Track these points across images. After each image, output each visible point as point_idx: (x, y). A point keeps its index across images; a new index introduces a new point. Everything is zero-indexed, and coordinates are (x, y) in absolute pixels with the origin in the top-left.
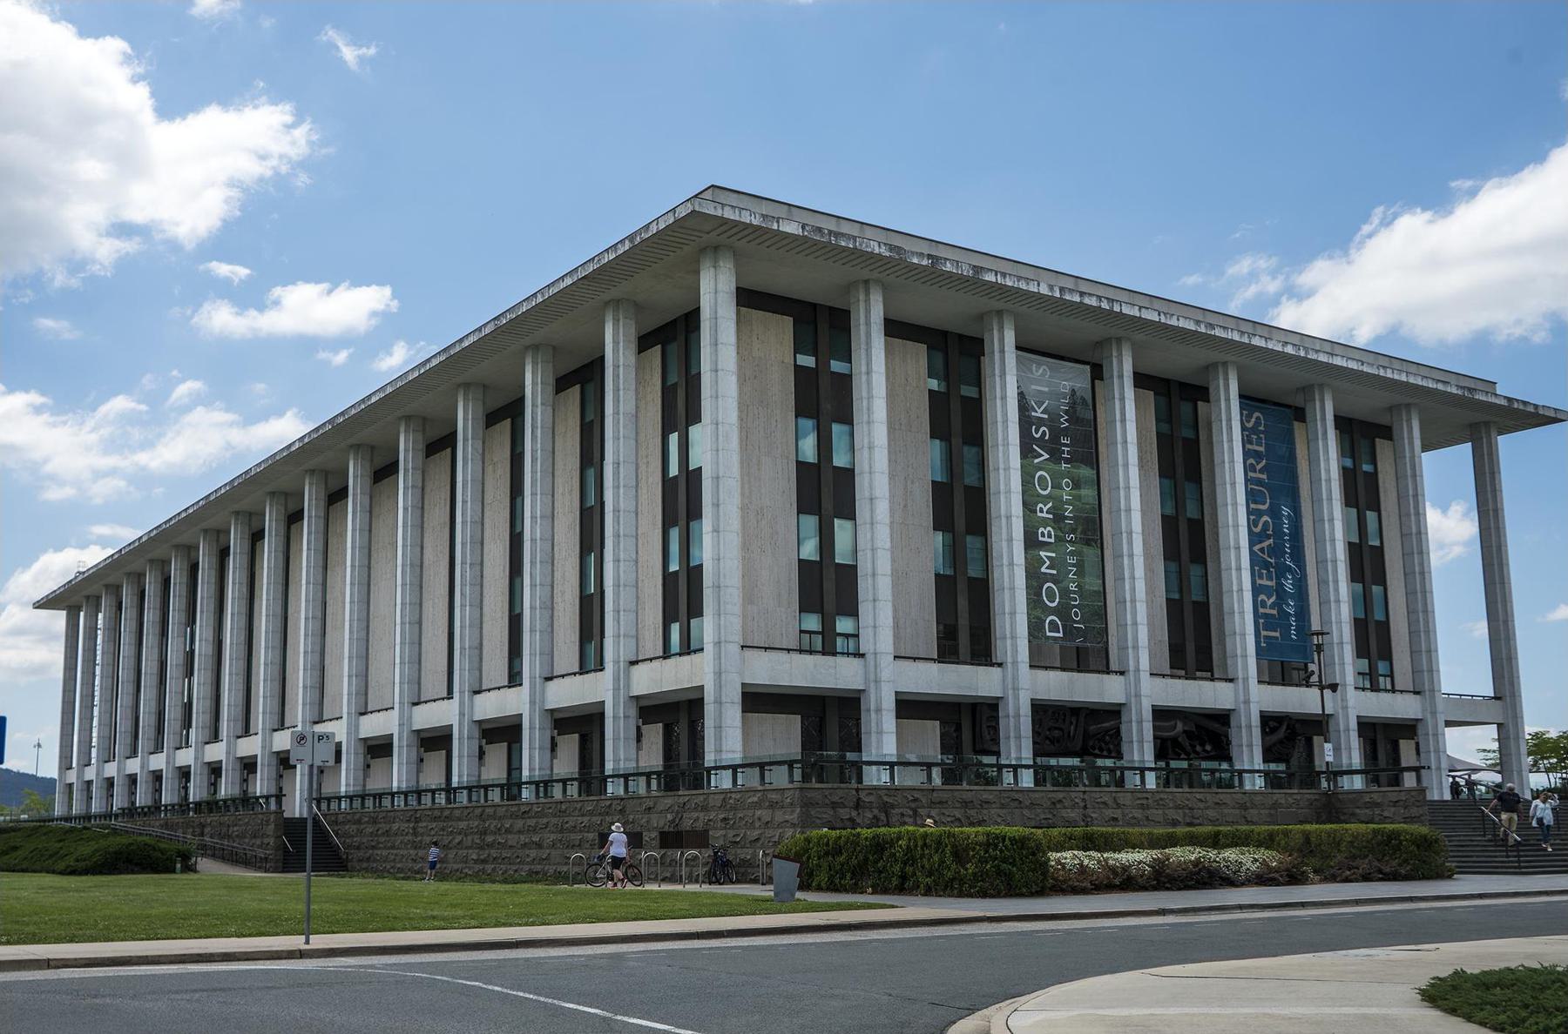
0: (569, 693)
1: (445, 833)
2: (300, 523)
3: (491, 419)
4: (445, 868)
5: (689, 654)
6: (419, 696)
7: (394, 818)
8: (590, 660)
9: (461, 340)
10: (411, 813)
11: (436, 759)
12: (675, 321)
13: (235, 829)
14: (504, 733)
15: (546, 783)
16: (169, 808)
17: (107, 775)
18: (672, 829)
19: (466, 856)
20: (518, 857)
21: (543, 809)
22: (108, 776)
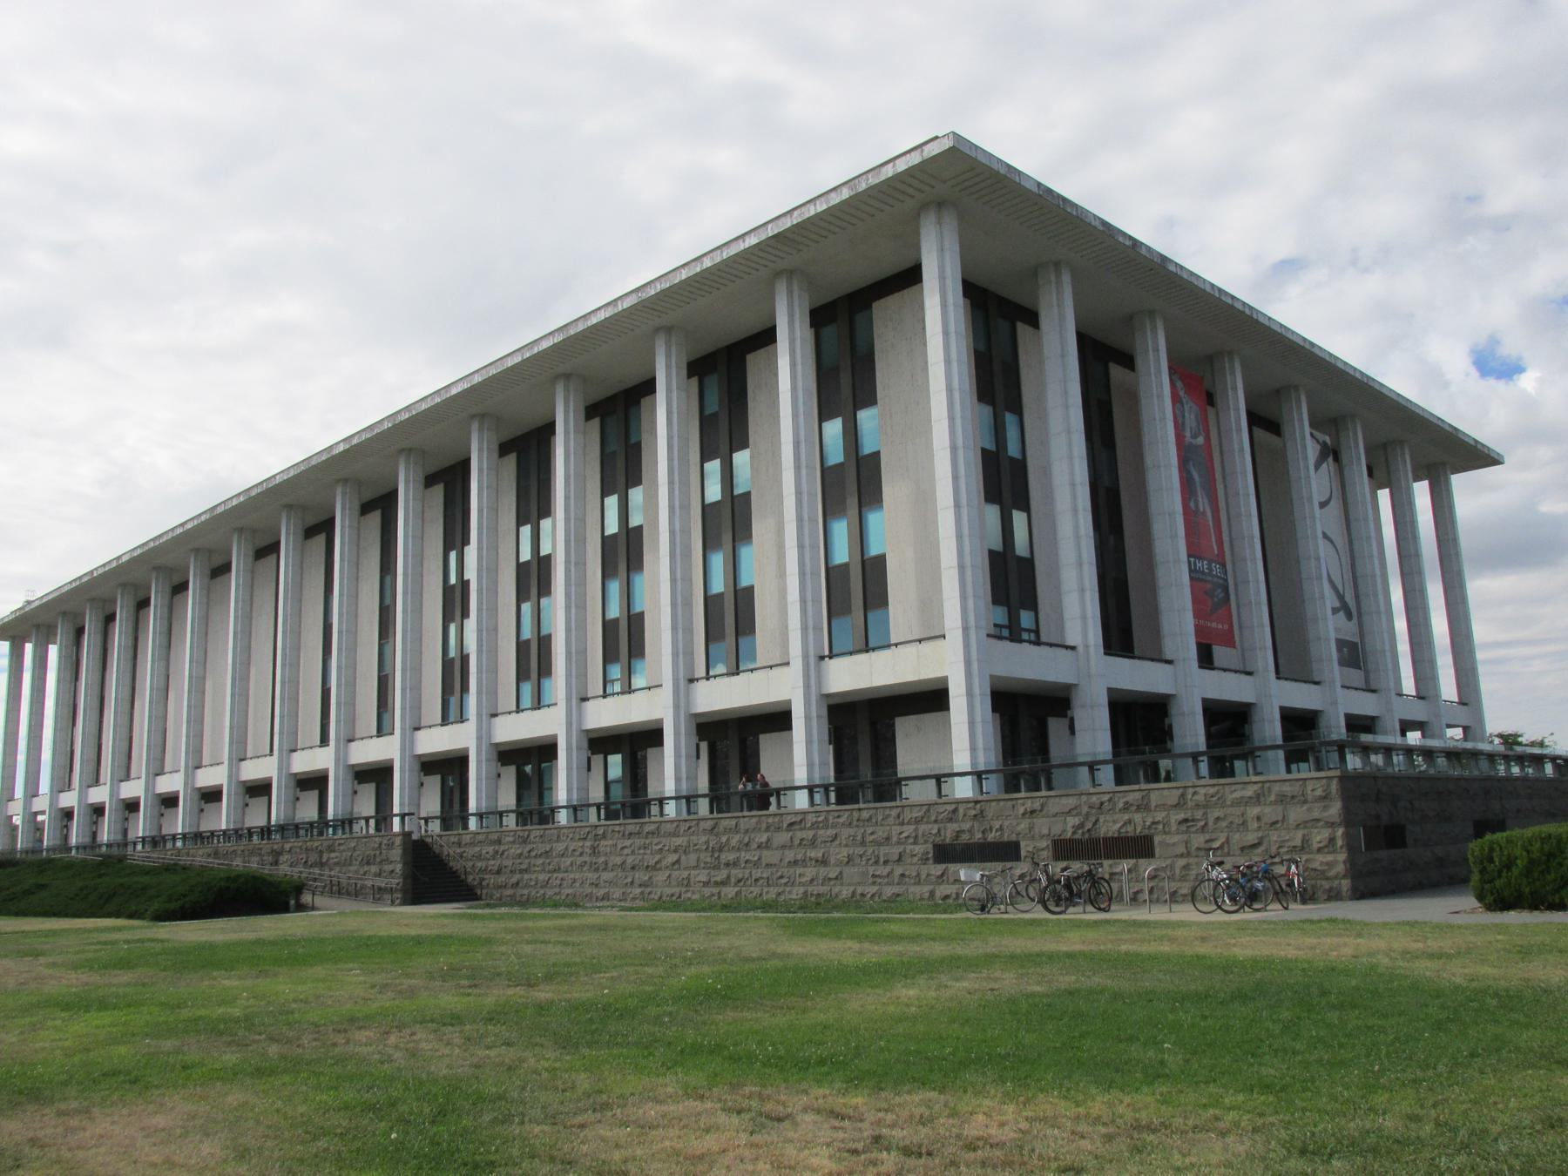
0: (436, 741)
1: (649, 852)
2: (227, 575)
3: (309, 533)
4: (650, 893)
5: (867, 651)
6: (420, 723)
7: (558, 836)
8: (451, 714)
9: (585, 317)
10: (587, 829)
11: (258, 804)
13: (333, 855)
14: (378, 775)
18: (1077, 836)
19: (688, 878)
20: (781, 877)
21: (826, 819)
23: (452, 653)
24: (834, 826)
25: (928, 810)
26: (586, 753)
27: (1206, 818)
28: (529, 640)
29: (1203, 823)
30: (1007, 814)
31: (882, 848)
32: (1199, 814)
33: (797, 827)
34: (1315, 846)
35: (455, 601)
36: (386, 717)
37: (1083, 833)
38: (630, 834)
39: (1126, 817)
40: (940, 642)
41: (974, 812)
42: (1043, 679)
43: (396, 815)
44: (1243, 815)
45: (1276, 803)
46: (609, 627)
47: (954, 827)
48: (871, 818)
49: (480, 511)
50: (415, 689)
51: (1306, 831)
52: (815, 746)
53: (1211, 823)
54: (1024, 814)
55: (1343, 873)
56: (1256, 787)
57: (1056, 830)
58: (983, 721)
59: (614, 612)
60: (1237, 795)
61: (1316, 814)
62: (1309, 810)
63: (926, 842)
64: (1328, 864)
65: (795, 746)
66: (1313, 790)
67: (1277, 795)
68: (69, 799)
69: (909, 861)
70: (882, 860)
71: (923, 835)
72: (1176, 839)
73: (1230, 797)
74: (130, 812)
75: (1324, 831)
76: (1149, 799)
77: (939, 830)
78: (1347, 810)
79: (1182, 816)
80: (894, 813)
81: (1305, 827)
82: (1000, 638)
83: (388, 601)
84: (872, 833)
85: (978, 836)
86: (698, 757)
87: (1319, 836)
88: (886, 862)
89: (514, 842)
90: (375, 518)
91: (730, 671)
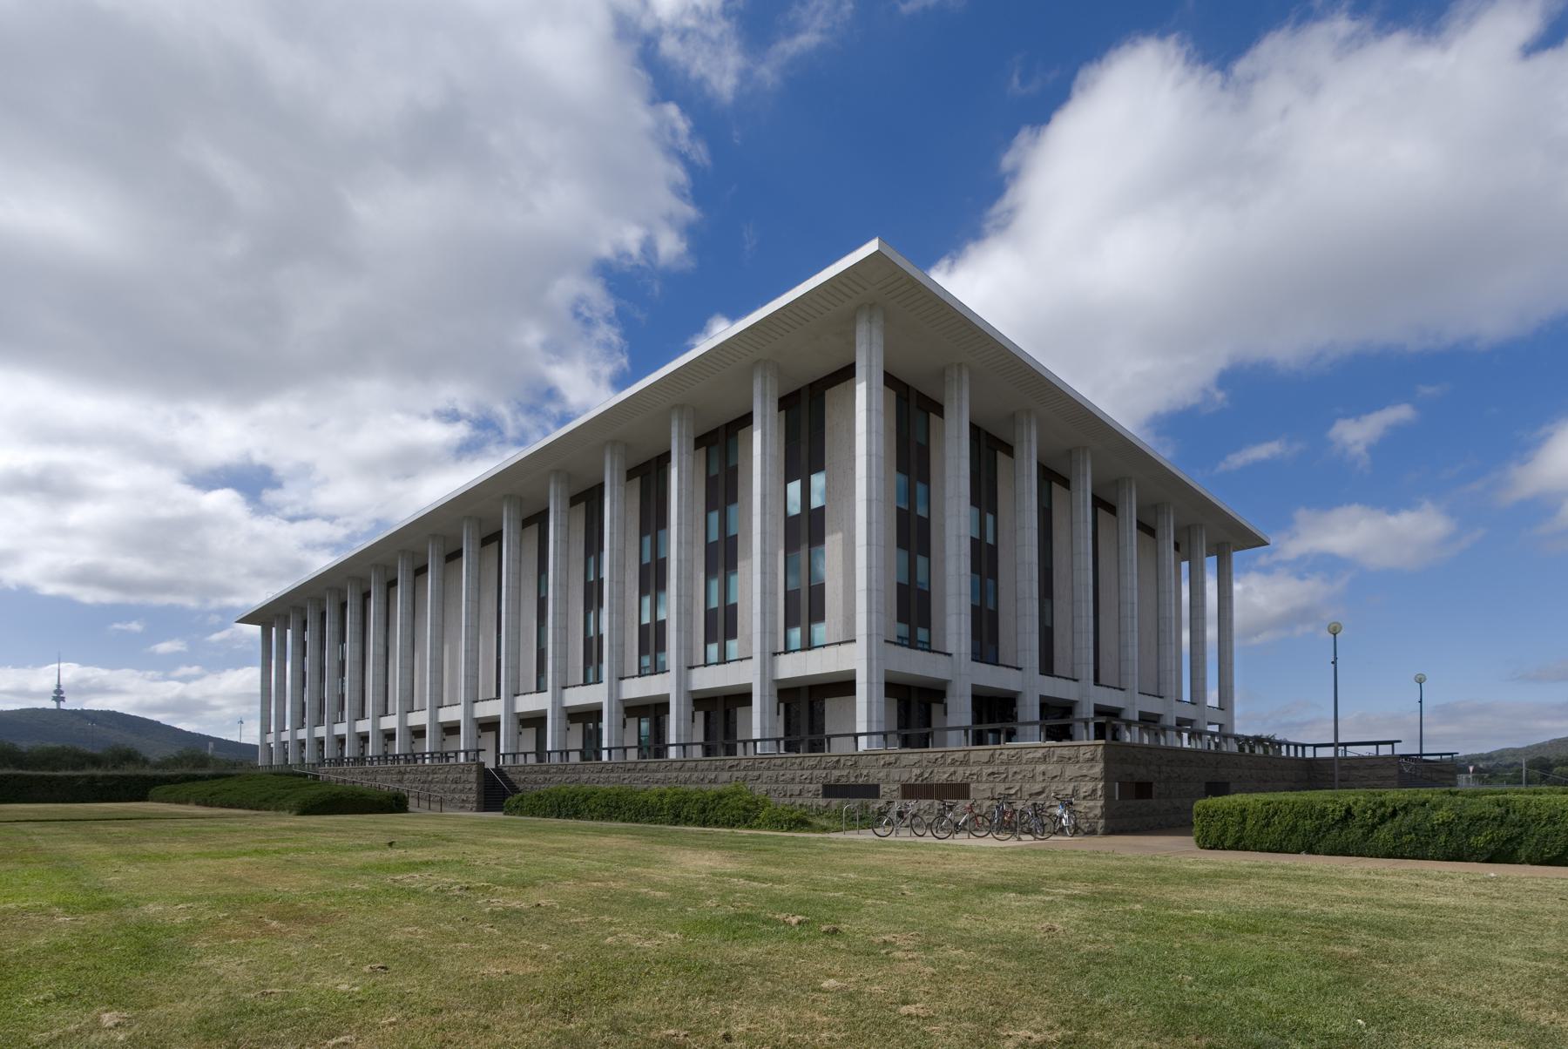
0: (579, 697)
5: (725, 663)
7: (584, 770)
8: (591, 675)
12: (717, 430)
13: (435, 776)
14: (535, 721)
15: (514, 755)
16: (351, 760)
17: (299, 737)
18: (917, 782)
21: (754, 764)
22: (319, 736)
23: (592, 632)
24: (759, 769)
25: (820, 760)
26: (691, 708)
27: (1008, 772)
28: (716, 609)
29: (1004, 775)
30: (873, 764)
31: (789, 785)
32: (1002, 769)
33: (735, 769)
34: (1082, 795)
36: (542, 680)
37: (922, 781)
38: (629, 770)
39: (952, 769)
41: (850, 763)
42: (926, 675)
43: (605, 749)
44: (1033, 770)
45: (1057, 762)
46: (710, 615)
47: (836, 773)
48: (783, 764)
49: (555, 542)
50: (563, 655)
51: (1076, 784)
52: (767, 716)
53: (1010, 776)
54: (883, 765)
55: (1099, 815)
56: (1044, 750)
57: (905, 777)
58: (877, 702)
59: (646, 620)
60: (1030, 756)
61: (1084, 772)
62: (1080, 768)
63: (818, 782)
64: (1089, 808)
65: (753, 714)
66: (1084, 754)
67: (1058, 757)
68: (303, 734)
69: (806, 795)
70: (788, 794)
71: (816, 778)
72: (985, 786)
73: (1025, 758)
74: (388, 740)
75: (1089, 784)
76: (969, 756)
77: (827, 774)
78: (1106, 770)
79: (990, 770)
80: (798, 761)
81: (1076, 781)
82: (902, 645)
83: (543, 595)
84: (783, 775)
85: (853, 779)
86: (778, 714)
87: (1085, 788)
88: (791, 796)
89: (556, 773)
90: (534, 530)
91: (803, 647)
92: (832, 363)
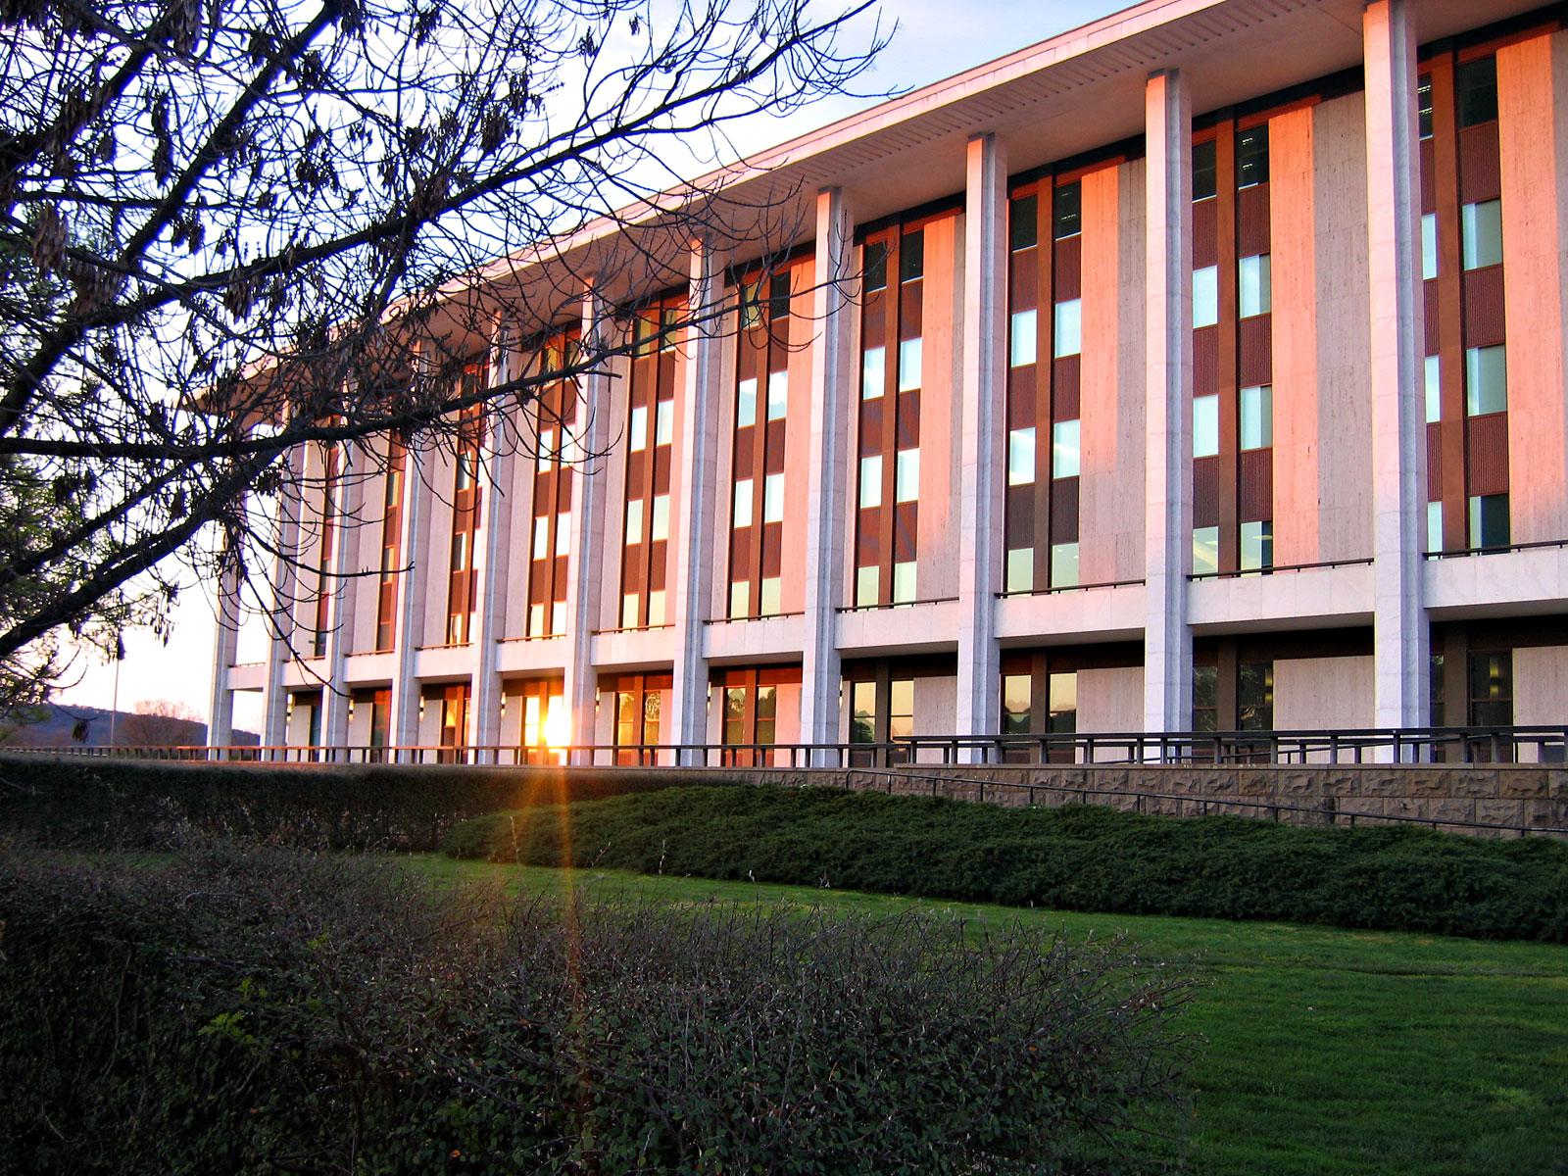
35: (465, 512)
40: (1138, 589)
83: (395, 502)
92: (925, 187)
